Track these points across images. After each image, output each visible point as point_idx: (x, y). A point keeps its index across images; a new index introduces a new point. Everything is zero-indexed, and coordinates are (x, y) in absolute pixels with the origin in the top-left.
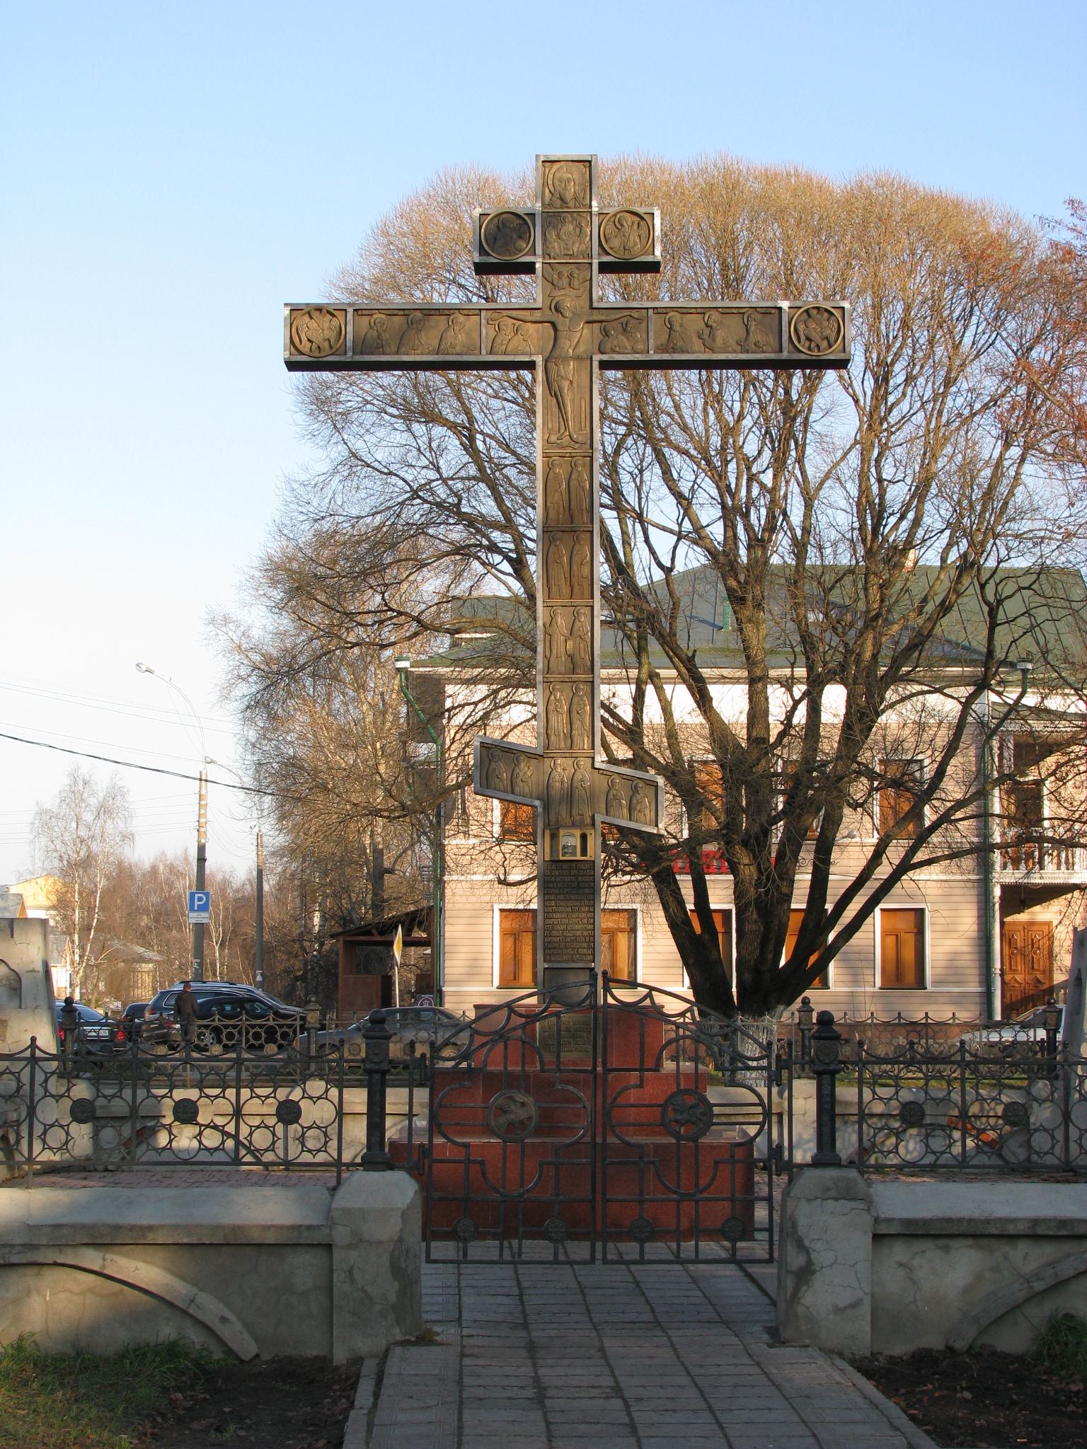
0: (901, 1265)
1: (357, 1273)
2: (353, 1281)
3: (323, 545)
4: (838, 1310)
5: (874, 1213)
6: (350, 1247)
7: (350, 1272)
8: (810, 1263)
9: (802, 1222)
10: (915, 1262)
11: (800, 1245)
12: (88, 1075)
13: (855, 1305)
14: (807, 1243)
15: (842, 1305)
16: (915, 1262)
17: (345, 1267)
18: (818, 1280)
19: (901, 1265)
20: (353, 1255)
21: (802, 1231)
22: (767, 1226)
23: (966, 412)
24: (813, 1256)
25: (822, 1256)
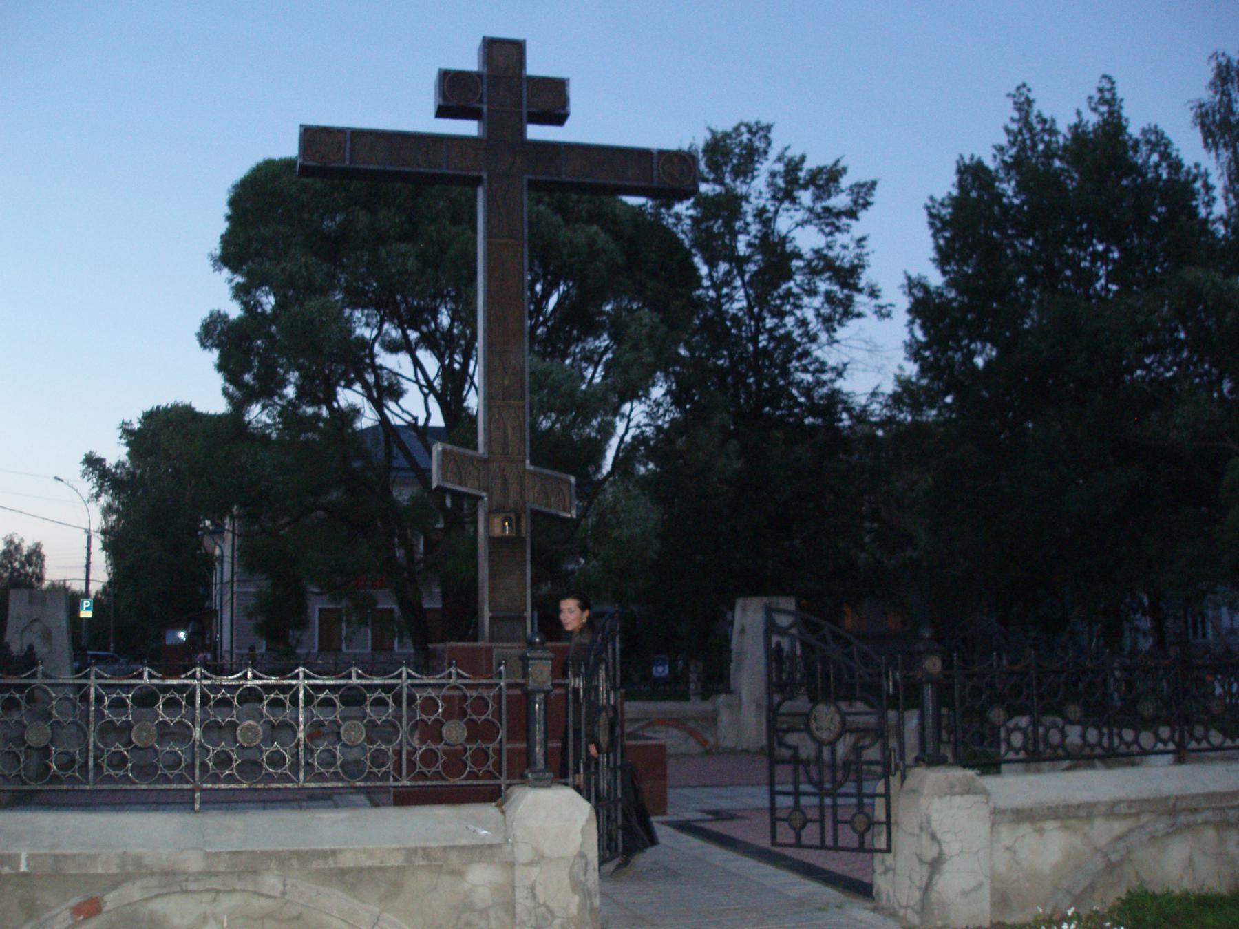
0: (1008, 849)
1: (539, 890)
2: (534, 896)
3: (1154, 146)
4: (964, 894)
5: (991, 804)
6: (532, 863)
7: (532, 888)
8: (941, 853)
9: (935, 817)
10: (1017, 846)
11: (933, 837)
12: (919, 335)
13: (980, 885)
14: (939, 836)
15: (967, 888)
16: (1017, 846)
17: (528, 884)
18: (947, 867)
19: (1008, 849)
20: (535, 870)
21: (935, 825)
22: (840, 826)
23: (191, 878)
24: (945, 847)
25: (952, 847)
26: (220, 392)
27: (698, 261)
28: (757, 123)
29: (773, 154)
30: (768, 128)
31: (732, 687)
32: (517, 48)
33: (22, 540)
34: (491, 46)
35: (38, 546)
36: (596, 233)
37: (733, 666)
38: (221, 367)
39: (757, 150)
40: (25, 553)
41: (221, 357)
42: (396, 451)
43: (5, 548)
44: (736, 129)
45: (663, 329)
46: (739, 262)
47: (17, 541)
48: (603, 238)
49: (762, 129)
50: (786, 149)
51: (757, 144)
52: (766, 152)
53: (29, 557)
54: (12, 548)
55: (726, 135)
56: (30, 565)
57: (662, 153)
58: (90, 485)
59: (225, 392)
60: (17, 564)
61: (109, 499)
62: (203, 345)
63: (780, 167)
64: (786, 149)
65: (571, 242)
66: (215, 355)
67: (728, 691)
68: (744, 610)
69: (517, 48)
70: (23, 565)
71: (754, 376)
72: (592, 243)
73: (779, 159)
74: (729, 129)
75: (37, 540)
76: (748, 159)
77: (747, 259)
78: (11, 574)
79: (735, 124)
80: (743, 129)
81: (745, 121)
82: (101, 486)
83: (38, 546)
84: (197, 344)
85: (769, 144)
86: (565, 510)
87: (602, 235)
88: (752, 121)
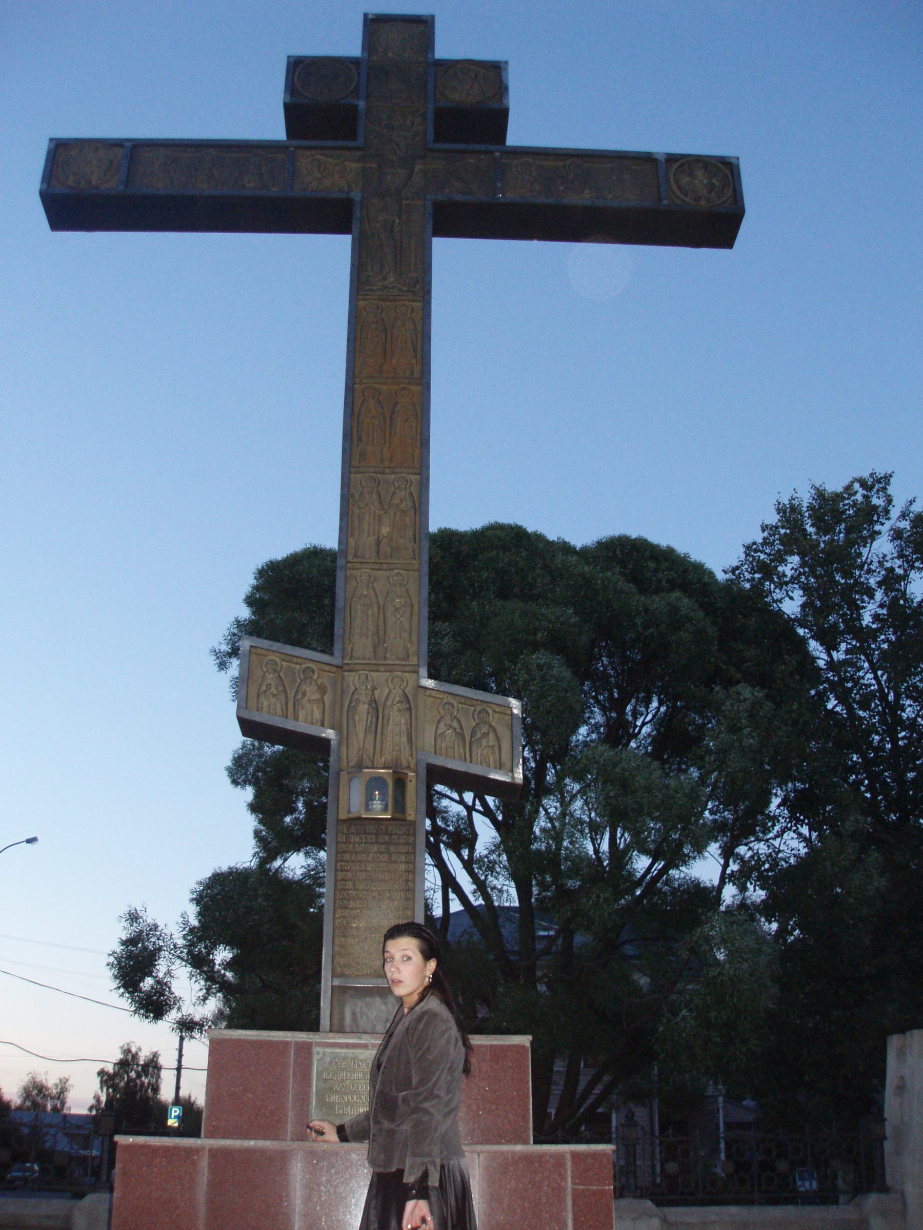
26: (252, 835)
27: (814, 646)
28: (871, 475)
29: (895, 513)
30: (887, 479)
31: (889, 1181)
32: (422, 26)
33: (140, 1049)
34: (375, 25)
35: (155, 1055)
36: (678, 599)
37: (888, 1145)
38: (254, 808)
39: (875, 508)
40: (142, 1062)
41: (257, 796)
42: (452, 896)
43: (122, 1056)
44: (848, 488)
45: (768, 705)
46: (864, 636)
47: (134, 1050)
48: (686, 603)
49: (879, 481)
50: (911, 502)
51: (875, 501)
52: (887, 512)
53: (146, 1066)
54: (130, 1057)
55: (838, 497)
56: (146, 1076)
57: (671, 159)
58: (197, 987)
59: (257, 834)
60: (133, 1074)
61: (220, 1005)
62: (235, 782)
63: (905, 524)
64: (911, 502)
65: (646, 610)
66: (248, 793)
67: (885, 1189)
68: (901, 1053)
69: (422, 26)
70: (139, 1076)
71: (897, 818)
72: (674, 610)
73: (904, 516)
74: (840, 489)
75: (154, 1050)
76: (868, 517)
77: (872, 634)
78: (127, 1083)
79: (846, 482)
80: (857, 486)
81: (857, 475)
82: (208, 990)
83: (155, 1055)
84: (228, 780)
85: (889, 501)
86: (500, 767)
87: (686, 600)
88: (865, 474)
